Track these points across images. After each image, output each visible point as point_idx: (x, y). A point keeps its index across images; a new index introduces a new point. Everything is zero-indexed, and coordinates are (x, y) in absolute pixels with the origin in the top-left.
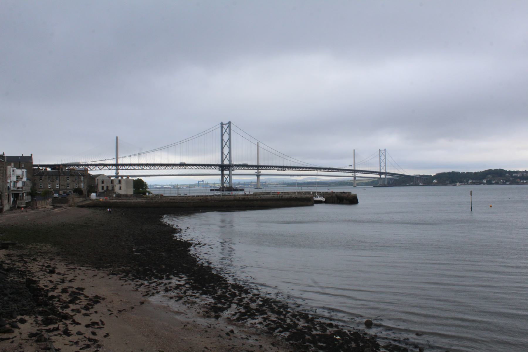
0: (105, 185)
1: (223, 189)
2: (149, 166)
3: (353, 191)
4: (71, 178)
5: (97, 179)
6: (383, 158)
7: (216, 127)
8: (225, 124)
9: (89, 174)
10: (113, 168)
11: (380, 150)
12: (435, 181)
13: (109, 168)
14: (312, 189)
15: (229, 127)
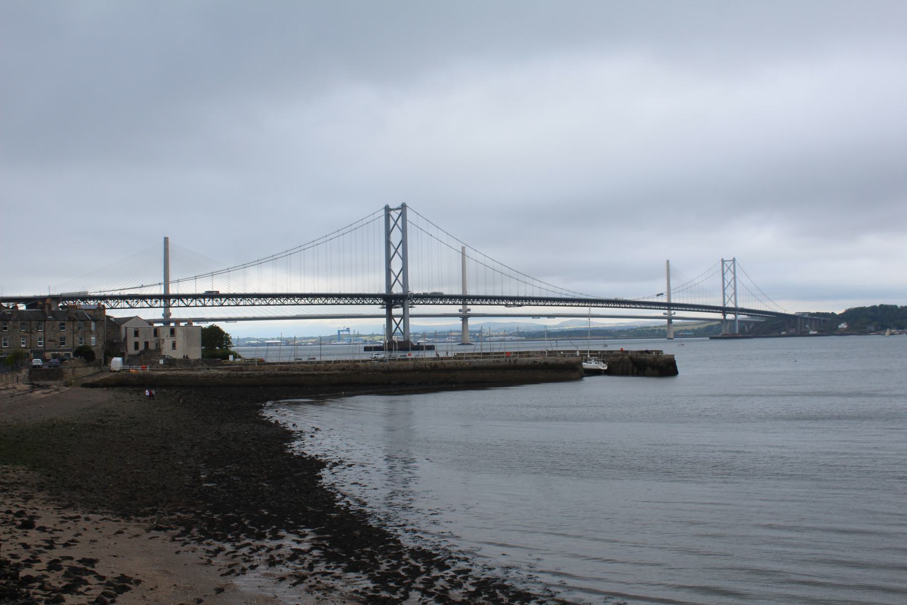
0: (141, 341)
1: (391, 346)
2: (234, 299)
3: (667, 348)
4: (69, 326)
5: (123, 326)
6: (729, 276)
7: (376, 215)
8: (394, 210)
9: (108, 317)
10: (159, 303)
11: (723, 261)
12: (843, 326)
13: (186, 302)
14: (580, 346)
15: (403, 215)
